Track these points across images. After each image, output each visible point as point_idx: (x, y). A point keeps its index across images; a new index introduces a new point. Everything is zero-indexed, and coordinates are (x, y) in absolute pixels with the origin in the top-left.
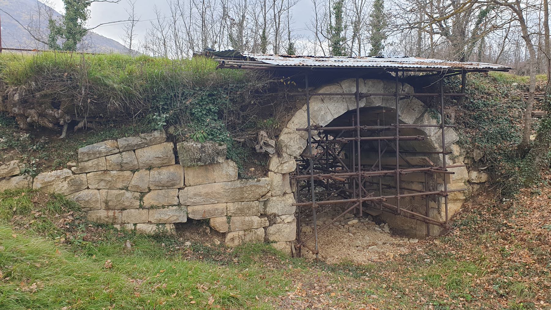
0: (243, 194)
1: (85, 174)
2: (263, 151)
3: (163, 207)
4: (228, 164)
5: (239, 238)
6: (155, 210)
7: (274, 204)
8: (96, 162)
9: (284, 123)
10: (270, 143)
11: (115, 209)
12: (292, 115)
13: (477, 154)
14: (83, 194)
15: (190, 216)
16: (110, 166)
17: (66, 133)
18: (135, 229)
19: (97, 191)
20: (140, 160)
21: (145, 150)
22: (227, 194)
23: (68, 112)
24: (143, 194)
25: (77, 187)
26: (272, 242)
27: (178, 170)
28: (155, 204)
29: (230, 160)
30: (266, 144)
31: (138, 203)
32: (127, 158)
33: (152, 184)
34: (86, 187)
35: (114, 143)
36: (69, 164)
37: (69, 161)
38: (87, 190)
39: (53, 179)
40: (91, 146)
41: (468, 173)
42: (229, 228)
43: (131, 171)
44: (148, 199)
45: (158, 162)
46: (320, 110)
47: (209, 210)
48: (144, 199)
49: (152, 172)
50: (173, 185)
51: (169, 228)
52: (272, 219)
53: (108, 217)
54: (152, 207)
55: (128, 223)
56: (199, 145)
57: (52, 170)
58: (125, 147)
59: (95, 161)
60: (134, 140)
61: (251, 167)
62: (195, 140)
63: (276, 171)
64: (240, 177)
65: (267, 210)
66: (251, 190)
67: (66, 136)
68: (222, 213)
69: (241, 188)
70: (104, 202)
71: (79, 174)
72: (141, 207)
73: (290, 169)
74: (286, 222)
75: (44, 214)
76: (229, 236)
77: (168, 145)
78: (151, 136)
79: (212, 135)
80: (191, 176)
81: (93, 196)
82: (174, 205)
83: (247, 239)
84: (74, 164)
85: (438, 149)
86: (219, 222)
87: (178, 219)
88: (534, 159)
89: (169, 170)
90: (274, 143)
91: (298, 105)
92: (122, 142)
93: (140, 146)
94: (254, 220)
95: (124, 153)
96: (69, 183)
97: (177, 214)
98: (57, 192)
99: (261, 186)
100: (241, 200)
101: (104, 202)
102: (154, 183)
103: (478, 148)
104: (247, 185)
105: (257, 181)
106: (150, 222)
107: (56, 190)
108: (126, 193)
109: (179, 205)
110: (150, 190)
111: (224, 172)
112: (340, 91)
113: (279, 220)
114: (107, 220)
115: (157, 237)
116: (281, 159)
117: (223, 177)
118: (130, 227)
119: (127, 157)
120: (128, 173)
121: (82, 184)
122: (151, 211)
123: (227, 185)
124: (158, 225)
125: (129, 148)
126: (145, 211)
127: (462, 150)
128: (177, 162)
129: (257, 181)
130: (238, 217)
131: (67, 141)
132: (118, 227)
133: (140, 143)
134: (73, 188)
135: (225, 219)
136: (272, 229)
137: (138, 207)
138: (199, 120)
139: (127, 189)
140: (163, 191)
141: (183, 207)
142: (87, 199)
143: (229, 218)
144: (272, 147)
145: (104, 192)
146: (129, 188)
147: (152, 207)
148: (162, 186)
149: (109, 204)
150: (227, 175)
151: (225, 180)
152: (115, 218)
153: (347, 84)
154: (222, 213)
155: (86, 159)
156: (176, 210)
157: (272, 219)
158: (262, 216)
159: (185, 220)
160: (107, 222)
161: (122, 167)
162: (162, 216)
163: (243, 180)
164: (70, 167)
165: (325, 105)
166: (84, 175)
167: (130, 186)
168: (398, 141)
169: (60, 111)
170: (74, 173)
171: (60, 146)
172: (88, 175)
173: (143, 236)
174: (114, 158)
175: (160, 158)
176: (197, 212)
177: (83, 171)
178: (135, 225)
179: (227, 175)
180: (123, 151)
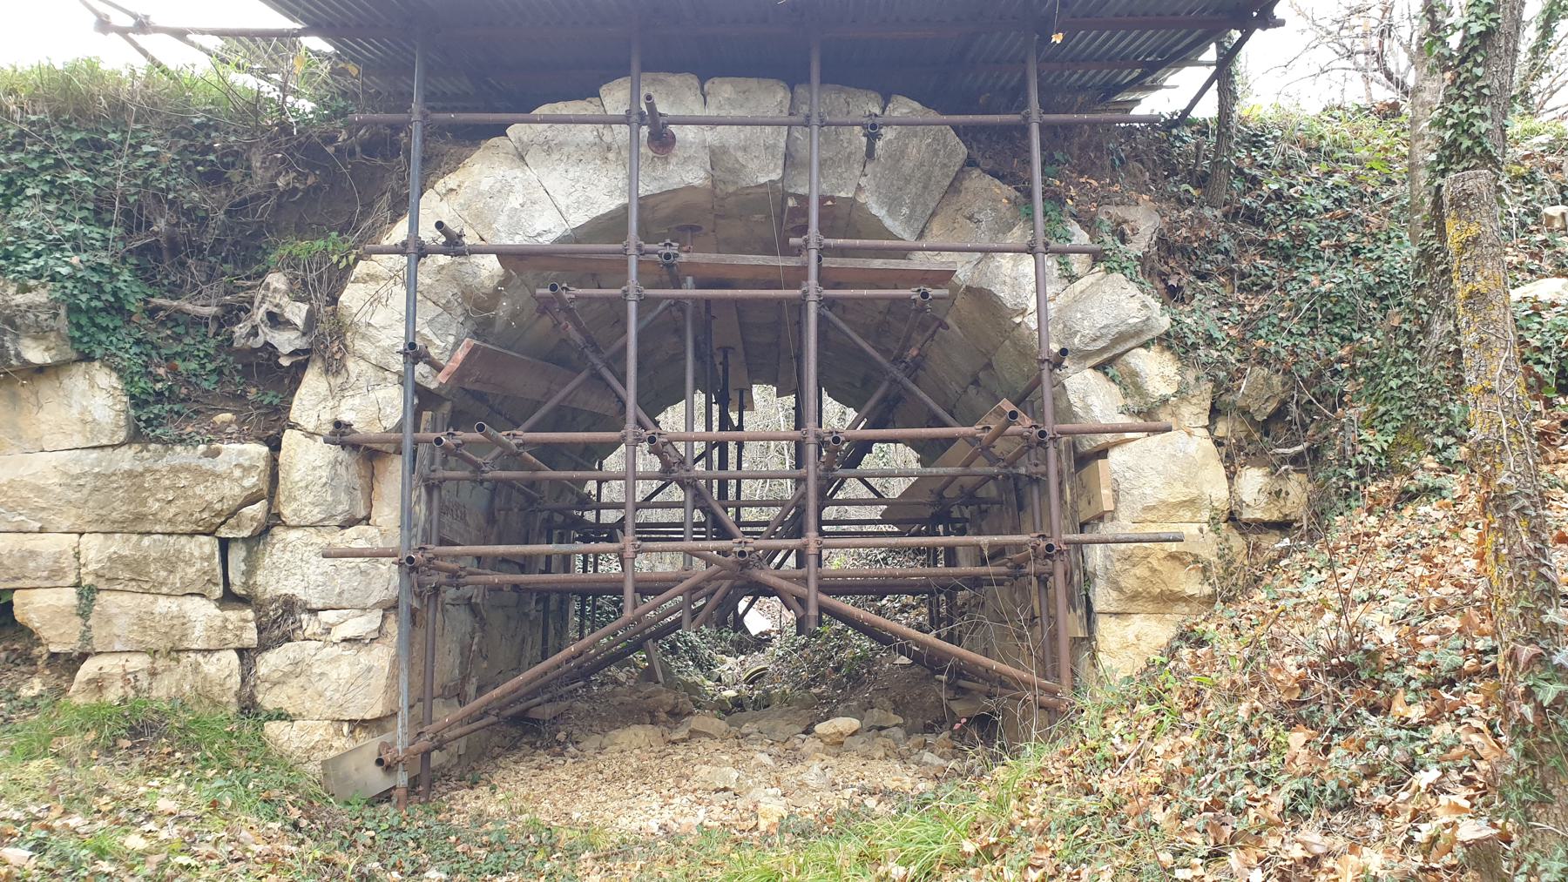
0: (144, 502)
4: (92, 379)
7: (287, 555)
10: (288, 315)
13: (1257, 388)
29: (97, 364)
41: (1231, 477)
42: (86, 637)
46: (505, 189)
52: (280, 621)
61: (223, 410)
64: (136, 436)
66: (173, 487)
69: (130, 474)
74: (337, 634)
83: (162, 690)
88: (1425, 330)
90: (303, 314)
100: (136, 525)
104: (160, 465)
105: (205, 455)
113: (311, 625)
117: (68, 429)
127: (1191, 375)
129: (205, 455)
130: (126, 596)
135: (69, 597)
136: (271, 662)
143: (87, 594)
150: (84, 422)
151: (78, 441)
157: (280, 621)
158: (230, 599)
163: (152, 446)
165: (532, 174)
179: (84, 422)
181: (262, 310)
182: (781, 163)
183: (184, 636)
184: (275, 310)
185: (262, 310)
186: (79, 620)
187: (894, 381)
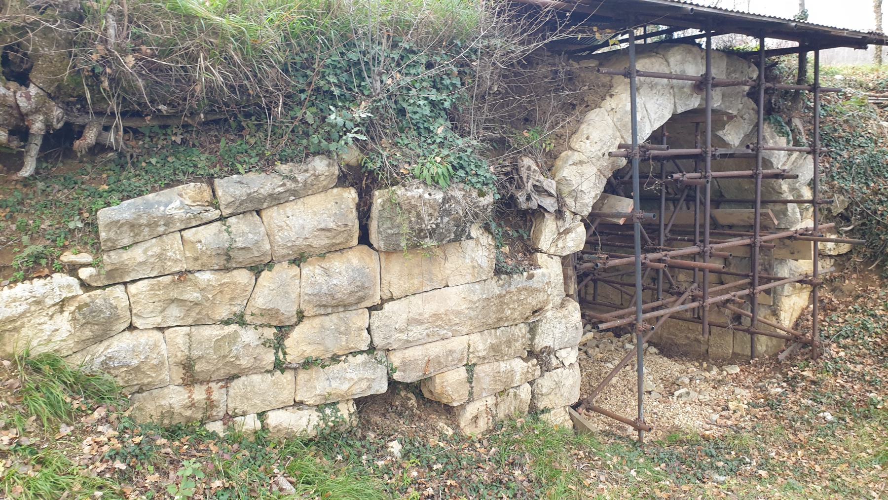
1: (122, 287)
2: (534, 205)
3: (335, 359)
5: (487, 413)
6: (314, 372)
8: (157, 250)
9: (563, 141)
10: (546, 188)
11: (208, 382)
12: (579, 122)
14: (121, 345)
15: (397, 376)
16: (196, 259)
17: (39, 160)
18: (264, 428)
19: (158, 335)
20: (278, 238)
21: (289, 208)
22: (473, 314)
23: (57, 93)
24: (283, 331)
25: (99, 326)
26: (543, 412)
27: (368, 260)
28: (314, 355)
30: (539, 190)
31: (269, 357)
32: (243, 234)
33: (309, 302)
34: (127, 325)
35: (202, 192)
36: (68, 257)
37: (65, 248)
38: (127, 334)
39: (21, 309)
40: (139, 200)
42: (471, 394)
43: (251, 269)
44: (298, 345)
45: (322, 242)
47: (438, 357)
48: (287, 342)
49: (307, 270)
50: (361, 300)
51: (346, 411)
53: (192, 405)
54: (308, 364)
55: (244, 414)
56: (439, 196)
57: (15, 282)
58: (241, 204)
59: (154, 247)
60: (263, 183)
62: (429, 181)
63: (552, 251)
65: (536, 341)
67: (37, 172)
68: (460, 360)
69: (500, 296)
70: (177, 364)
71: (104, 287)
72: (280, 366)
73: (578, 246)
75: (26, 433)
76: (471, 410)
77: (346, 195)
78: (306, 171)
79: (457, 170)
80: (396, 275)
81: (152, 350)
82: (361, 352)
84: (85, 257)
85: (785, 195)
86: (450, 383)
87: (369, 387)
89: (349, 261)
91: (589, 98)
92: (229, 188)
93: (276, 200)
94: (516, 369)
95: (233, 220)
96: (74, 319)
97: (369, 374)
98: (38, 350)
99: (537, 290)
101: (177, 364)
102: (315, 299)
103: (841, 190)
104: (513, 288)
106: (299, 404)
107: (35, 343)
108: (242, 331)
109: (372, 349)
110: (301, 316)
111: (468, 261)
112: (665, 70)
114: (188, 413)
115: (325, 441)
116: (560, 223)
117: (464, 272)
118: (251, 423)
119: (243, 231)
120: (243, 277)
121: (114, 317)
122: (303, 375)
123: (474, 292)
124: (319, 408)
125: (250, 206)
126: (289, 375)
128: (364, 239)
131: (41, 185)
132: (217, 427)
133: (281, 189)
134: (87, 333)
137: (271, 367)
138: (423, 131)
139: (240, 320)
140: (334, 317)
141: (380, 354)
142: (135, 362)
143: (470, 368)
144: (550, 195)
145: (179, 336)
146: (248, 318)
147: (308, 364)
148: (334, 305)
149: (198, 367)
150: (474, 267)
151: (469, 278)
152: (211, 404)
153: (679, 57)
154: (460, 360)
155: (126, 241)
156: (365, 364)
159: (382, 387)
160: (189, 419)
161: (229, 258)
162: (335, 384)
163: (503, 276)
164: (72, 269)
166: (119, 290)
167: (248, 312)
168: (759, 181)
169: (33, 90)
170: (86, 286)
171: (21, 203)
172: (132, 288)
173: (294, 446)
174: (208, 236)
175: (329, 230)
176: (409, 363)
177: (116, 278)
178: (261, 415)
179: (474, 267)
180: (231, 215)
181: (530, 184)
182: (721, 97)
183: (512, 381)
184: (537, 184)
185: (530, 184)
186: (468, 385)
187: (706, 153)
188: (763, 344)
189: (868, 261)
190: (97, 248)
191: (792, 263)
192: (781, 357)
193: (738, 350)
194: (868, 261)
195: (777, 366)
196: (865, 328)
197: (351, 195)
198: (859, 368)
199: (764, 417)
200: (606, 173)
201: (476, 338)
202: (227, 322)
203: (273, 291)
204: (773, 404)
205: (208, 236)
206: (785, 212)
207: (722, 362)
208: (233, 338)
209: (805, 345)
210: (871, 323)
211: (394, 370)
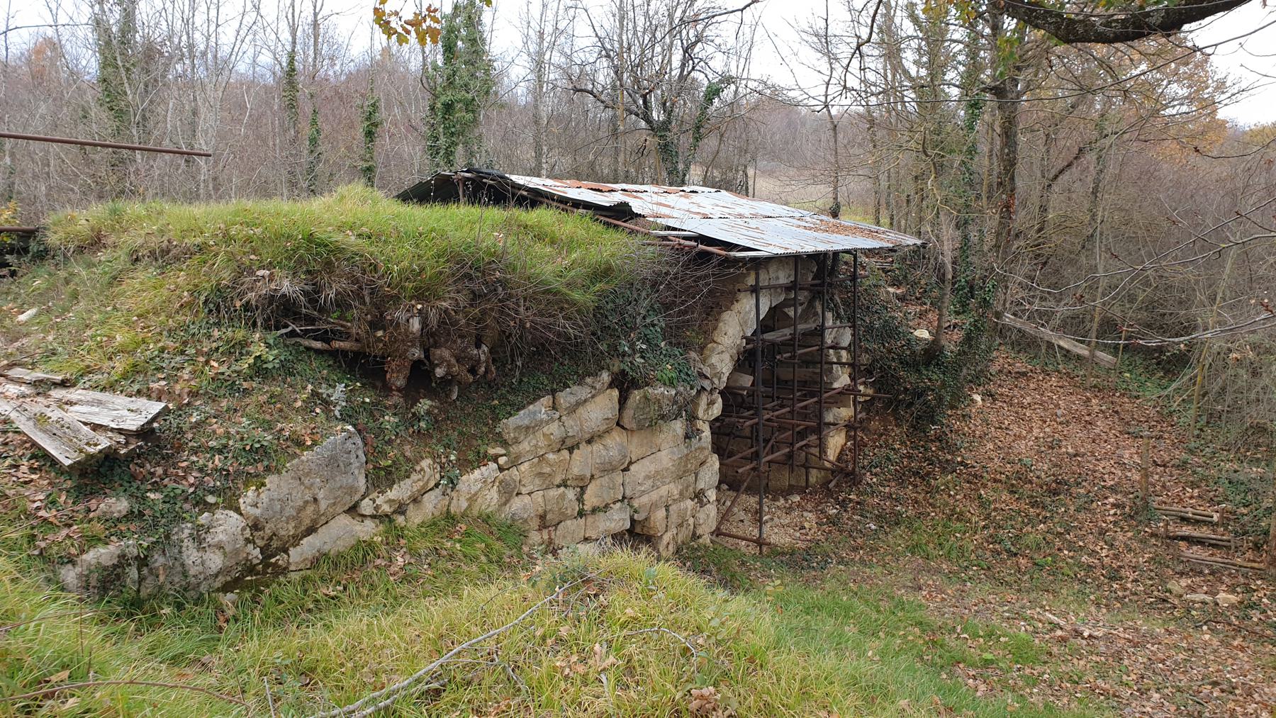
14: (517, 504)
25: (509, 491)
44: (591, 499)
48: (585, 497)
54: (594, 510)
72: (581, 514)
92: (565, 398)
139: (564, 484)
143: (667, 508)
145: (538, 496)
164: (495, 459)
188: (814, 476)
189: (887, 407)
190: (505, 444)
191: (835, 410)
192: (831, 486)
193: (793, 483)
194: (887, 407)
195: (829, 493)
196: (889, 459)
197: (616, 393)
198: (887, 489)
199: (830, 532)
200: (12, 50)
201: (672, 485)
202: (558, 486)
203: (580, 462)
204: (833, 521)
205: (554, 429)
206: (831, 371)
207: (787, 492)
208: (563, 496)
209: (847, 475)
210: (892, 455)
211: (636, 511)
